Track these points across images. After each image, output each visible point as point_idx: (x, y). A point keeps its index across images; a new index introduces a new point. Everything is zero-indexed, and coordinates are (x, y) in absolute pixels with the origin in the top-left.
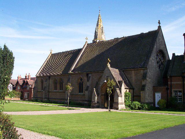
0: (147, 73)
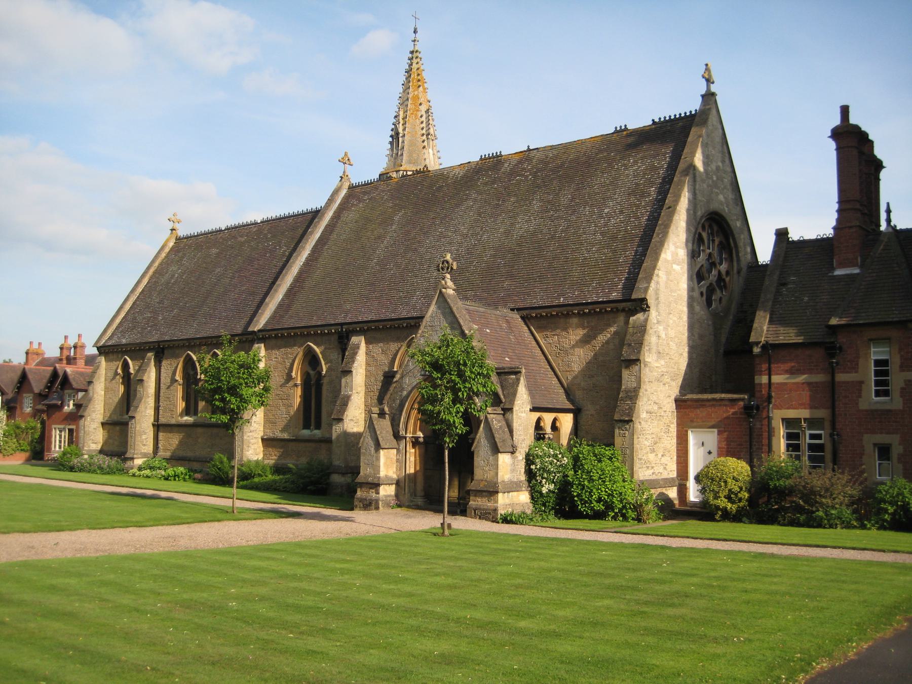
0: (645, 326)
